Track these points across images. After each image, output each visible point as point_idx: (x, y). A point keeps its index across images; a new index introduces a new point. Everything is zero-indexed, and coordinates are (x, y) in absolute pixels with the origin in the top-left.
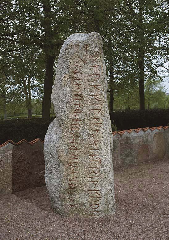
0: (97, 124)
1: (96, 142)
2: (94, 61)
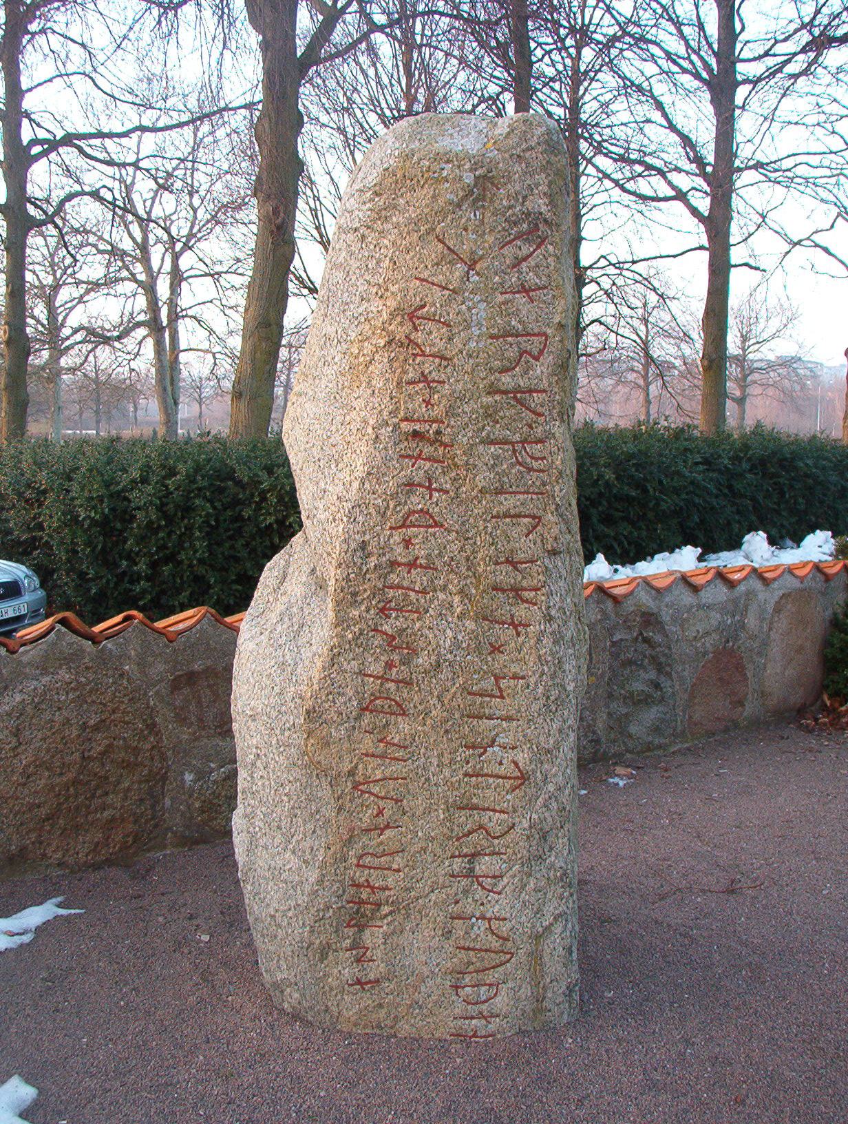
0: (516, 590)
1: (503, 683)
2: (518, 262)
